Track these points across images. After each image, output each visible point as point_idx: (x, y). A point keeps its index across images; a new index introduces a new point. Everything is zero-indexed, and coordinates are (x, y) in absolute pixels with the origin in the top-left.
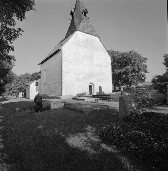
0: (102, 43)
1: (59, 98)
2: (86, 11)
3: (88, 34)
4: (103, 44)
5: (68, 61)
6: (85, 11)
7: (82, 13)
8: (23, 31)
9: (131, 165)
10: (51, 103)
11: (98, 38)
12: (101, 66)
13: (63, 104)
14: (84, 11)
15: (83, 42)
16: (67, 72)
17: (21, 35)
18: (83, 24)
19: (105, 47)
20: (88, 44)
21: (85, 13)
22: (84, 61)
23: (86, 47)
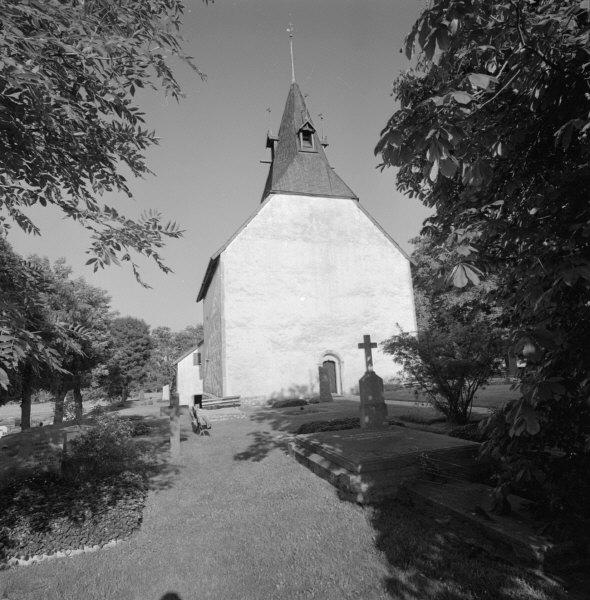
0: (367, 214)
1: (234, 406)
2: (310, 126)
3: (312, 195)
4: (373, 220)
5: (242, 289)
6: (307, 128)
7: (298, 134)
8: (106, 292)
9: (74, 443)
10: (409, 254)
11: (351, 202)
12: (367, 293)
13: (252, 437)
14: (301, 130)
15: (295, 224)
16: (240, 325)
17: (96, 270)
18: (295, 171)
19: (381, 228)
20: (315, 228)
21: (307, 134)
22: (299, 282)
23: (306, 240)
